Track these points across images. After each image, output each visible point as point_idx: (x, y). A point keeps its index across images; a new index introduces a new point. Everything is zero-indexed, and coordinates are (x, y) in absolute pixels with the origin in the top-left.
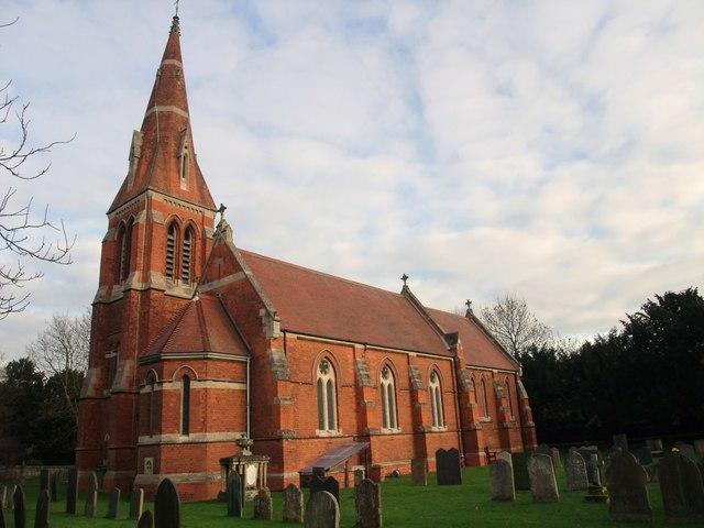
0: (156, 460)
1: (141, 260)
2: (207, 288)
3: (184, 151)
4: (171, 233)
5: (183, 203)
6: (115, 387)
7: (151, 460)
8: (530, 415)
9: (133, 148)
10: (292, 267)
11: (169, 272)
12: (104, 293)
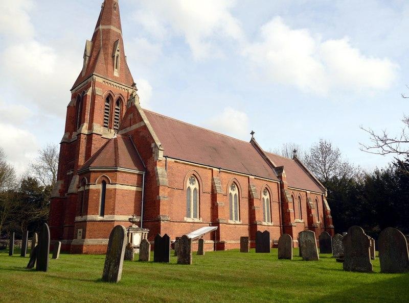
0: (83, 231)
1: (87, 117)
2: (124, 132)
3: (117, 53)
4: (108, 102)
5: (115, 84)
6: (70, 191)
7: (81, 230)
8: (331, 221)
9: (86, 51)
10: (178, 122)
11: (106, 125)
12: (67, 136)
